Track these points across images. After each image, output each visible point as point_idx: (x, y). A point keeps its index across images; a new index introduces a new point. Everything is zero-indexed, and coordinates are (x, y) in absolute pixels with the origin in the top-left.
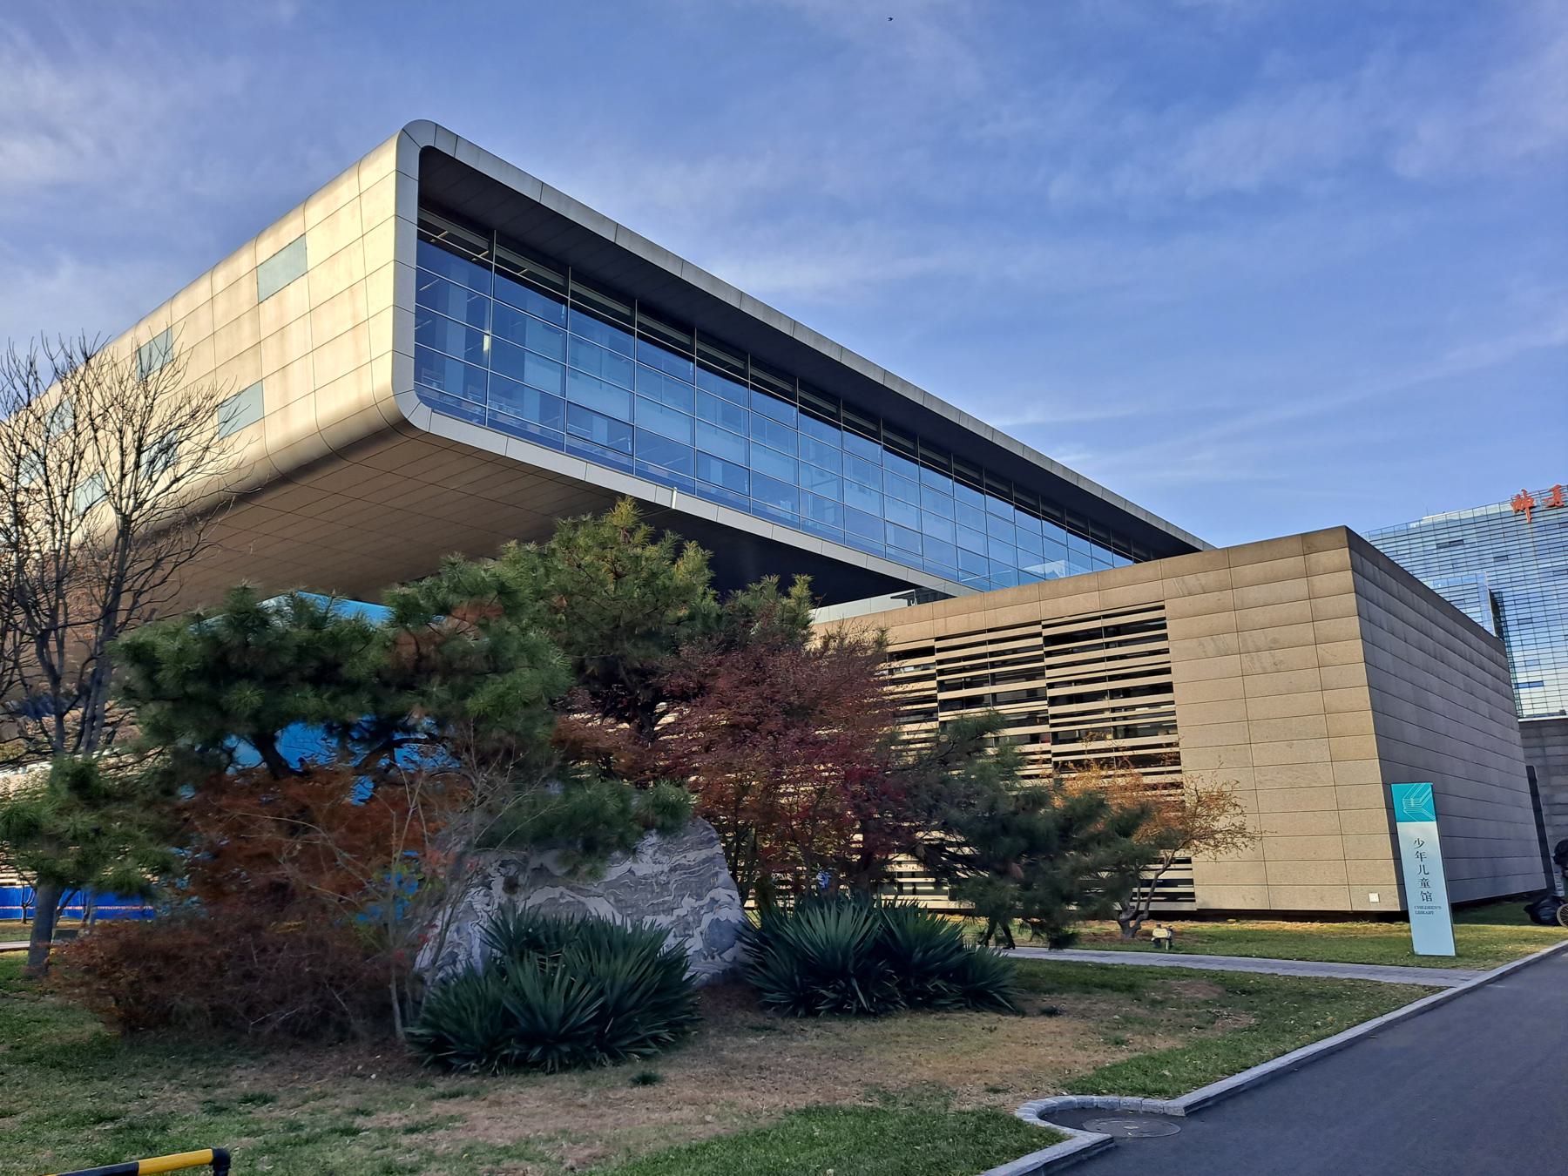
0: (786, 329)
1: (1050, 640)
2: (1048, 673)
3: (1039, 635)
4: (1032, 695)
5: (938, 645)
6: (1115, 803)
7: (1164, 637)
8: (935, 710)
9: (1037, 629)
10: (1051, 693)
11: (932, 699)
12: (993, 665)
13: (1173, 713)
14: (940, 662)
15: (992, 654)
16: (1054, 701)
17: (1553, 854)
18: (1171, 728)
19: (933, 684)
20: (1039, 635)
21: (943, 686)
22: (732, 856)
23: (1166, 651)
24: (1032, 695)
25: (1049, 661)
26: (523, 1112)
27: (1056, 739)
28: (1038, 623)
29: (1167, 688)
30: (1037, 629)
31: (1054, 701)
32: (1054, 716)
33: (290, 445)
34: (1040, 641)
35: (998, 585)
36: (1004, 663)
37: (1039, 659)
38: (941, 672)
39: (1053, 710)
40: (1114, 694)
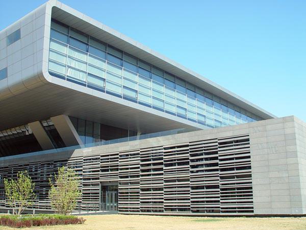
2: (219, 152)
3: (217, 142)
5: (190, 144)
7: (249, 144)
12: (205, 150)
13: (250, 164)
14: (190, 149)
18: (250, 168)
19: (188, 155)
20: (217, 142)
22: (6, 130)
23: (249, 147)
28: (118, 154)
29: (249, 157)
31: (221, 160)
32: (220, 164)
33: (23, 83)
34: (217, 144)
35: (230, 124)
36: (156, 156)
38: (191, 152)
40: (237, 158)
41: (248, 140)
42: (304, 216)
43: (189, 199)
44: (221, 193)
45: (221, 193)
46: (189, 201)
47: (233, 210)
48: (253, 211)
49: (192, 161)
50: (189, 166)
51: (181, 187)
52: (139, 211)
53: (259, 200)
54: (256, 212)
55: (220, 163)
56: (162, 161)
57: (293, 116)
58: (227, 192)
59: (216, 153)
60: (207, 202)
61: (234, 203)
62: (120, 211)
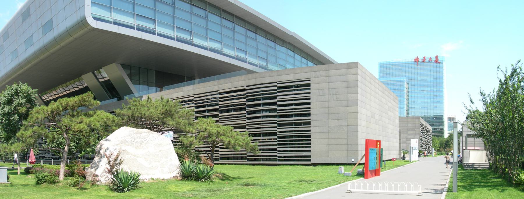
4: (275, 104)
7: (309, 89)
9: (275, 84)
10: (278, 103)
19: (245, 100)
24: (275, 104)
25: (278, 94)
30: (275, 84)
34: (276, 88)
39: (278, 108)
41: (309, 85)
44: (279, 141)
45: (279, 141)
48: (310, 160)
49: (249, 106)
50: (245, 112)
55: (278, 108)
56: (217, 107)
57: (357, 63)
58: (284, 141)
59: (275, 98)
61: (290, 151)
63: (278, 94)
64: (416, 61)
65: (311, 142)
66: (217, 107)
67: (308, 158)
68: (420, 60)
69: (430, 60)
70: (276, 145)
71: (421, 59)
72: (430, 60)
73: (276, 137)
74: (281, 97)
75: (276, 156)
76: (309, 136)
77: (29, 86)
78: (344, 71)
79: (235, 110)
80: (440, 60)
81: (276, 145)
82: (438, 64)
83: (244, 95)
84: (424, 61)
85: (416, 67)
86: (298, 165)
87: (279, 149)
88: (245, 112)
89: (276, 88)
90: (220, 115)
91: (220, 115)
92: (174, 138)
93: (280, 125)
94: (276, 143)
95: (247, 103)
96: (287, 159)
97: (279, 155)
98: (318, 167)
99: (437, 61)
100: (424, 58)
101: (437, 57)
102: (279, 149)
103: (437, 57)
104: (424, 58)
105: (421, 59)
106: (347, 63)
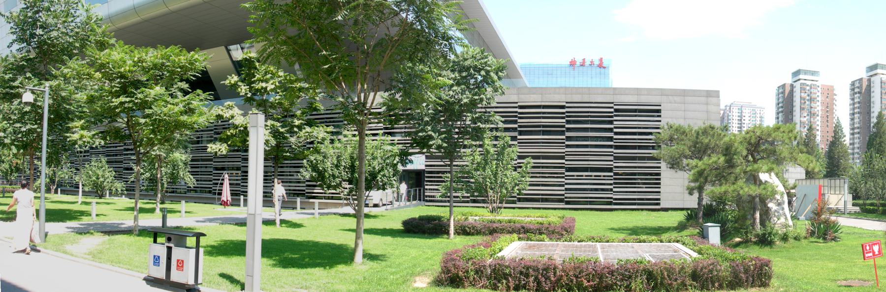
0: (135, 19)
1: (616, 110)
4: (610, 130)
6: (51, 101)
7: (660, 116)
8: (563, 131)
9: (612, 105)
10: (615, 130)
11: (564, 126)
15: (636, 116)
16: (616, 134)
17: (833, 218)
19: (564, 121)
21: (568, 122)
24: (610, 130)
25: (615, 118)
26: (317, 273)
27: (617, 147)
30: (612, 105)
31: (616, 134)
34: (612, 110)
37: (611, 117)
39: (615, 137)
41: (659, 111)
42: (884, 267)
43: (563, 186)
44: (615, 179)
45: (615, 179)
46: (563, 188)
47: (632, 202)
48: (658, 204)
49: (569, 130)
50: (564, 137)
51: (543, 167)
52: (468, 202)
53: (577, 233)
54: (662, 206)
55: (615, 137)
56: (516, 126)
57: (718, 92)
58: (627, 179)
59: (611, 122)
60: (592, 190)
61: (639, 191)
62: (427, 201)
63: (615, 118)
64: (573, 63)
65: (661, 181)
66: (516, 126)
67: (657, 202)
68: (578, 64)
69: (592, 63)
70: (611, 184)
71: (579, 61)
72: (592, 63)
73: (612, 174)
74: (619, 122)
75: (611, 198)
76: (659, 174)
77: (126, 44)
78: (703, 99)
79: (545, 133)
80: (605, 65)
81: (611, 184)
82: (603, 70)
83: (563, 113)
84: (583, 65)
85: (572, 72)
86: (642, 210)
87: (615, 190)
88: (564, 137)
89: (612, 110)
90: (519, 137)
91: (519, 137)
92: (426, 166)
93: (616, 158)
94: (612, 182)
95: (567, 126)
96: (632, 202)
97: (615, 197)
98: (670, 212)
99: (601, 66)
100: (584, 60)
101: (601, 60)
102: (615, 190)
103: (601, 60)
104: (584, 60)
105: (579, 61)
106: (707, 91)
